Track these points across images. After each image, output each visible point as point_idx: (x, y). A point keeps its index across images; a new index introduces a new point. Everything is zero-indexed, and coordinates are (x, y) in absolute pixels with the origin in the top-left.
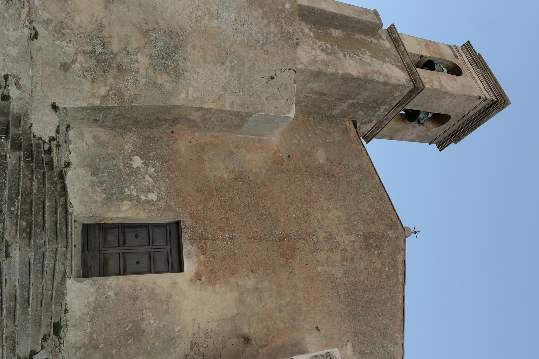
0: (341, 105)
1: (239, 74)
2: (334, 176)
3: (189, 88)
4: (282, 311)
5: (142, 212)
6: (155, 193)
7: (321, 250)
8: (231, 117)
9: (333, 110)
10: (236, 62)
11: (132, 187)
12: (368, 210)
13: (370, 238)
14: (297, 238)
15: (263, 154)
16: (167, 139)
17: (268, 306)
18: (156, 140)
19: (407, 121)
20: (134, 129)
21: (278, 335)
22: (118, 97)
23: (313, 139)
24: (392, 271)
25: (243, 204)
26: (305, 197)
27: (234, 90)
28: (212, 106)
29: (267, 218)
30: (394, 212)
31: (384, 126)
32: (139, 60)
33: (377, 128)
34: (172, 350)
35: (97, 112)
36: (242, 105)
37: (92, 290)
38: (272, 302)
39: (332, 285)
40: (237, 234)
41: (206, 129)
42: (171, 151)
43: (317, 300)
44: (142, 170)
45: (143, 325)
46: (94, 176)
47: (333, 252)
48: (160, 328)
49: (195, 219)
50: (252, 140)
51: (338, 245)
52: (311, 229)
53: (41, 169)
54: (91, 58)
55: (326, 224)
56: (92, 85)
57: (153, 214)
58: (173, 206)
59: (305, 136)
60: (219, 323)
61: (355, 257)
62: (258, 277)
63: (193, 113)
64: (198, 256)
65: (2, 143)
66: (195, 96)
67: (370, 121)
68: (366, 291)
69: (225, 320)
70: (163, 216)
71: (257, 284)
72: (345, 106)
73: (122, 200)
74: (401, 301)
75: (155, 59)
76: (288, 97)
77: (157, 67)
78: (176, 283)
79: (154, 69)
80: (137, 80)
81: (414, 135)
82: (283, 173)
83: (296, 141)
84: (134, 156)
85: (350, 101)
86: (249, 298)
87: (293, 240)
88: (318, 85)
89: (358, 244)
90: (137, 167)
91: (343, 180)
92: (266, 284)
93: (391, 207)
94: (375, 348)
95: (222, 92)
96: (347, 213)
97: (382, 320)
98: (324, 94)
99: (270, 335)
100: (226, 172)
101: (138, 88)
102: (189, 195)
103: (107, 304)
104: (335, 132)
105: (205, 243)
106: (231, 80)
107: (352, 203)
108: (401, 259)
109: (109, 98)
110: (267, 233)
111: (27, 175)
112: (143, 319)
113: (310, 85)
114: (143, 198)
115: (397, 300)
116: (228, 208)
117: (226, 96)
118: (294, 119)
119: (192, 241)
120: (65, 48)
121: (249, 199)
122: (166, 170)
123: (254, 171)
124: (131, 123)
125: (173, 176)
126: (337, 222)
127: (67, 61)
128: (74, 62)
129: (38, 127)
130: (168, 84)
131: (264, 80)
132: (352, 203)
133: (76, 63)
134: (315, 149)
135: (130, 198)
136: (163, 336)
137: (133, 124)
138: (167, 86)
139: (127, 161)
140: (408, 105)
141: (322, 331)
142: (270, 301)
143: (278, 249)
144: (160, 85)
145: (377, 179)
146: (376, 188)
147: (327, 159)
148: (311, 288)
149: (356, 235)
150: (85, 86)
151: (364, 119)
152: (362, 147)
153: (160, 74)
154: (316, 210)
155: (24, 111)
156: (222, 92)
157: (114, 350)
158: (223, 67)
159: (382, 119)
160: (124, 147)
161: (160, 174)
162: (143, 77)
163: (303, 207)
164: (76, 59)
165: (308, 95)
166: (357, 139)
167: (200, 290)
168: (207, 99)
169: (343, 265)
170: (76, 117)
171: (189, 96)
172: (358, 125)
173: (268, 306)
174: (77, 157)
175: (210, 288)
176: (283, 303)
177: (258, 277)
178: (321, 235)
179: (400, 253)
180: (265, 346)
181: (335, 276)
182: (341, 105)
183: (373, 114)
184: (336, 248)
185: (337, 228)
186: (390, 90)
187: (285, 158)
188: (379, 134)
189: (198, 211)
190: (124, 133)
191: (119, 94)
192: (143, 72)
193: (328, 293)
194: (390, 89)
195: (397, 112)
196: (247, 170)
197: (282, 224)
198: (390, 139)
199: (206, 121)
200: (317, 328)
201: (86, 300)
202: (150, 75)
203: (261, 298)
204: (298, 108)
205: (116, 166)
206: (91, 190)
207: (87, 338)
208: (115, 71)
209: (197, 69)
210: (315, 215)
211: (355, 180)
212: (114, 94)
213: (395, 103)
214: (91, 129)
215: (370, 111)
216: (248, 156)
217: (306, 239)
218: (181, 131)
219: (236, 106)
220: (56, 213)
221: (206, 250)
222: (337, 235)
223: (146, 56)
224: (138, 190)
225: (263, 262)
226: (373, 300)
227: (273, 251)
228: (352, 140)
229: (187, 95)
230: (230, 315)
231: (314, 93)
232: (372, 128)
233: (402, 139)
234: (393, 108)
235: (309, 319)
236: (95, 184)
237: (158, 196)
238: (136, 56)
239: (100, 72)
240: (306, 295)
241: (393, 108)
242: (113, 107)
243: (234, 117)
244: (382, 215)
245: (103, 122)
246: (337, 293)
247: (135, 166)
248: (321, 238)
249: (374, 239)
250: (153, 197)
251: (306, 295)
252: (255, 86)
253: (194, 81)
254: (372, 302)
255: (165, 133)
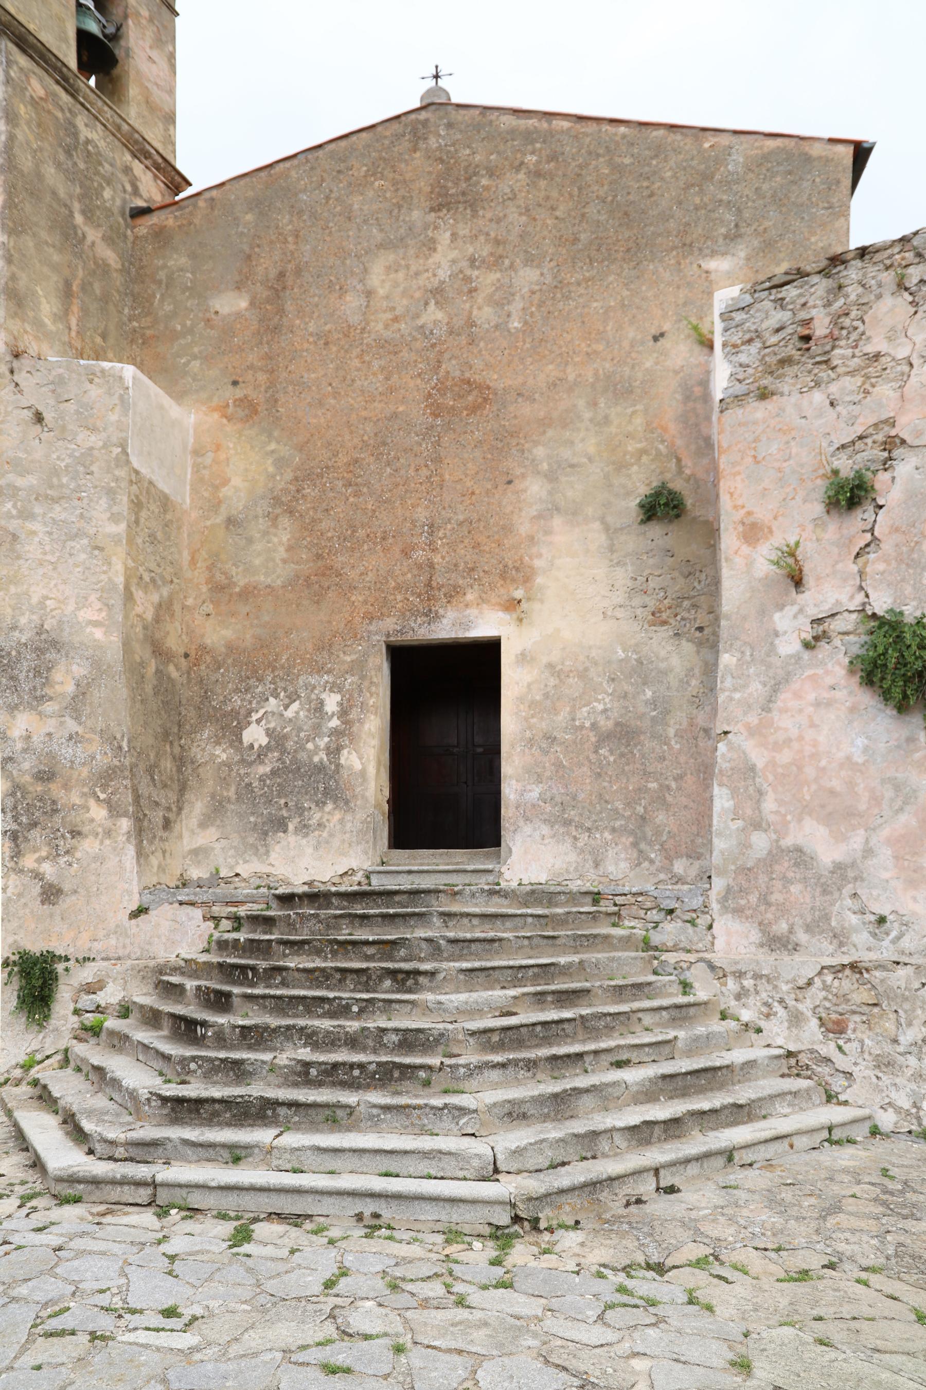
0: (93, 243)
1: (36, 499)
2: (282, 275)
3: (80, 619)
4: (606, 417)
5: (367, 726)
6: (323, 696)
7: (469, 318)
8: (142, 520)
9: (108, 265)
10: (9, 505)
11: (310, 746)
12: (371, 194)
13: (446, 195)
14: (437, 374)
15: (231, 445)
16: (203, 667)
17: (592, 450)
18: (206, 692)
19: (116, 72)
20: (183, 741)
21: (659, 431)
22: (111, 780)
23: (189, 323)
24: (538, 145)
25: (351, 499)
26: (334, 349)
27: (78, 512)
28: (118, 566)
29: (384, 444)
30: (379, 129)
31: (136, 136)
32: (24, 733)
33: (147, 155)
34: (663, 665)
35: (146, 823)
36: (111, 493)
37: (527, 829)
38: (583, 440)
39: (559, 295)
40: (422, 514)
41: (175, 580)
42: (230, 661)
43: (590, 333)
44: (272, 725)
45: (606, 724)
46: (286, 826)
47: (476, 290)
48: (614, 690)
49: (385, 610)
50: (198, 471)
51: (461, 276)
52: (416, 340)
53: (270, 947)
54: (26, 839)
55: (405, 302)
56: (86, 836)
57: (371, 703)
58: (354, 657)
59: (182, 342)
60: (618, 563)
61: (493, 234)
62: (523, 470)
63: (139, 609)
64: (467, 606)
65: (214, 1033)
66: (98, 605)
67: (127, 170)
68: (583, 215)
69: (612, 549)
70: (375, 680)
71: (539, 473)
72: (93, 235)
73: (338, 766)
74: (622, 129)
75: (19, 697)
76: (83, 378)
77: (38, 693)
78: (523, 654)
79: (42, 699)
80: (70, 738)
81: (155, 54)
82: (276, 401)
83: (196, 365)
84: (241, 742)
85: (79, 219)
86: (570, 494)
87: (442, 383)
88: (43, 300)
89: (460, 225)
90: (268, 735)
91: (292, 253)
92: (540, 452)
93: (364, 135)
94: (729, 202)
95: (85, 541)
96: (380, 246)
97: (662, 179)
98: (68, 284)
99: (657, 449)
100: (275, 535)
101: (87, 736)
102: (329, 622)
103: (558, 799)
104: (165, 266)
105: (439, 589)
106: (53, 519)
107: (351, 233)
108: (508, 121)
109: (115, 798)
110: (421, 445)
111: (283, 979)
112: (594, 726)
113: (46, 320)
114: (335, 723)
115: (617, 138)
116: (361, 533)
117: (92, 531)
118: (140, 366)
119: (431, 616)
120: (9, 894)
121: (340, 483)
122: (273, 671)
123: (271, 469)
124: (168, 748)
125: (285, 657)
126: (401, 275)
127: (37, 890)
128: (38, 876)
129: (184, 945)
130: (75, 668)
131: (45, 436)
132: (351, 233)
133: (41, 870)
134: (213, 316)
135: (334, 751)
136: (632, 684)
137: (171, 743)
138: (79, 670)
139: (253, 758)
140: (65, 61)
141: (666, 327)
142: (580, 445)
143: (461, 420)
144: (78, 685)
145: (287, 164)
146: (312, 169)
147: (238, 288)
148: (560, 347)
149: (436, 228)
150: (89, 850)
151: (123, 187)
152: (203, 197)
153: (52, 687)
154: (368, 324)
155: (150, 975)
156: (85, 541)
157: (651, 785)
158: (23, 536)
159: (119, 140)
160: (224, 764)
161: (281, 684)
162: (62, 723)
163: (360, 356)
164: (32, 871)
165: (74, 327)
166: (182, 209)
167: (542, 601)
168: (103, 577)
169: (512, 266)
170: (159, 866)
171: (100, 618)
172: (141, 204)
173: (592, 450)
174: (246, 862)
175: (539, 580)
176: (587, 415)
177: (523, 470)
178: (433, 314)
179: (491, 122)
180: (679, 460)
181: (537, 288)
182: (93, 243)
183: (106, 161)
184: (468, 279)
185: (417, 274)
186: (29, 107)
187: (239, 393)
188: (161, 151)
189: (365, 602)
190: (193, 762)
191: (106, 777)
192: (51, 725)
193: (576, 308)
194: (26, 107)
195: (92, 96)
196: (270, 485)
197: (401, 409)
198: (174, 122)
199: (157, 578)
200: (656, 339)
201: (546, 841)
202: (57, 708)
203: (572, 466)
204: (110, 355)
205: (264, 781)
206: (317, 833)
207: (624, 839)
208: (53, 786)
209: (35, 600)
210: (380, 326)
211: (291, 222)
212: (104, 787)
213: (65, 97)
214: (186, 834)
215: (100, 168)
216: (236, 481)
217: (441, 353)
218: (184, 637)
219: (116, 509)
220: (364, 917)
221: (455, 587)
222: (435, 275)
223: (14, 717)
224: (317, 730)
225: (489, 456)
226: (610, 198)
227: (465, 433)
228: (185, 222)
229: (96, 624)
230: (603, 537)
231: (67, 312)
232: (147, 167)
233: (171, 92)
234: (82, 105)
235: (633, 355)
236: (305, 826)
237: (331, 691)
238: (14, 741)
239: (57, 819)
240: (577, 359)
241: (82, 105)
242: (135, 790)
243: (144, 514)
244: (385, 159)
245: (169, 809)
246: (579, 284)
247: (264, 741)
248: (440, 315)
249: (450, 184)
250: (332, 702)
251: (577, 359)
252: (63, 460)
253: (63, 606)
254: (612, 201)
255: (189, 673)
